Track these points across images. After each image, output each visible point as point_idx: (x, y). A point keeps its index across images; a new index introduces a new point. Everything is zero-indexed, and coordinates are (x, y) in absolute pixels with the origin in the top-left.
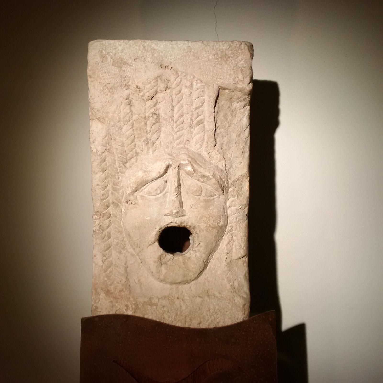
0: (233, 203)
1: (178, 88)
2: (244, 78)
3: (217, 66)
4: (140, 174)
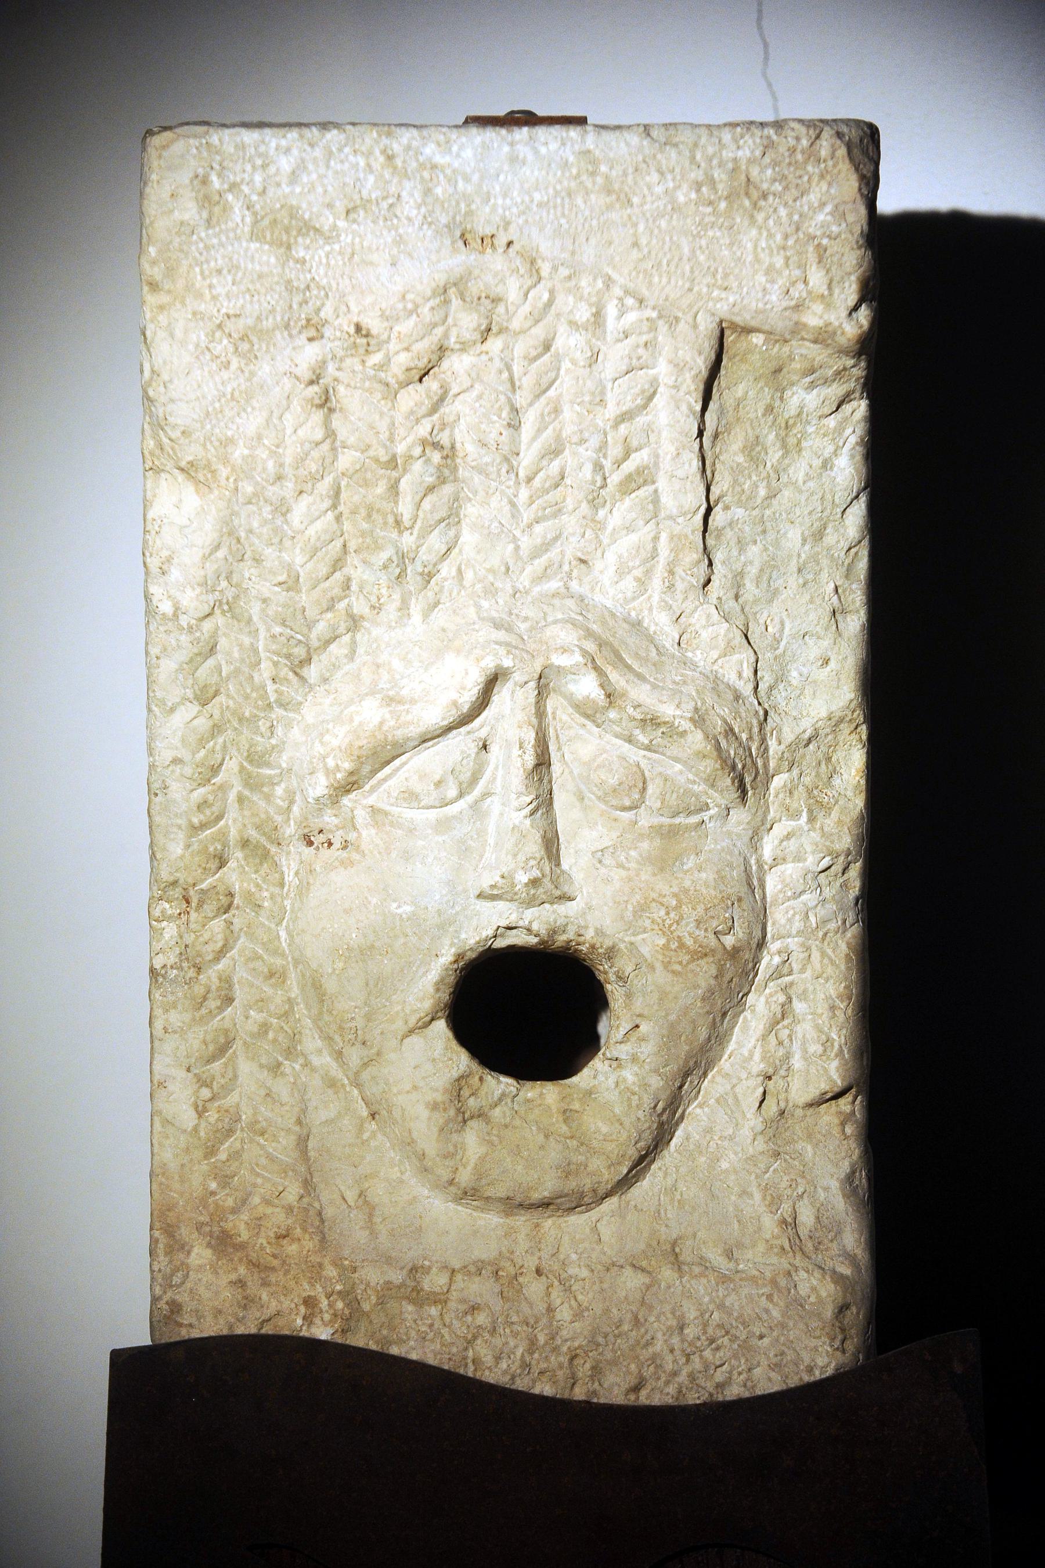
0: (792, 845)
1: (539, 332)
2: (834, 283)
3: (710, 233)
4: (371, 714)
